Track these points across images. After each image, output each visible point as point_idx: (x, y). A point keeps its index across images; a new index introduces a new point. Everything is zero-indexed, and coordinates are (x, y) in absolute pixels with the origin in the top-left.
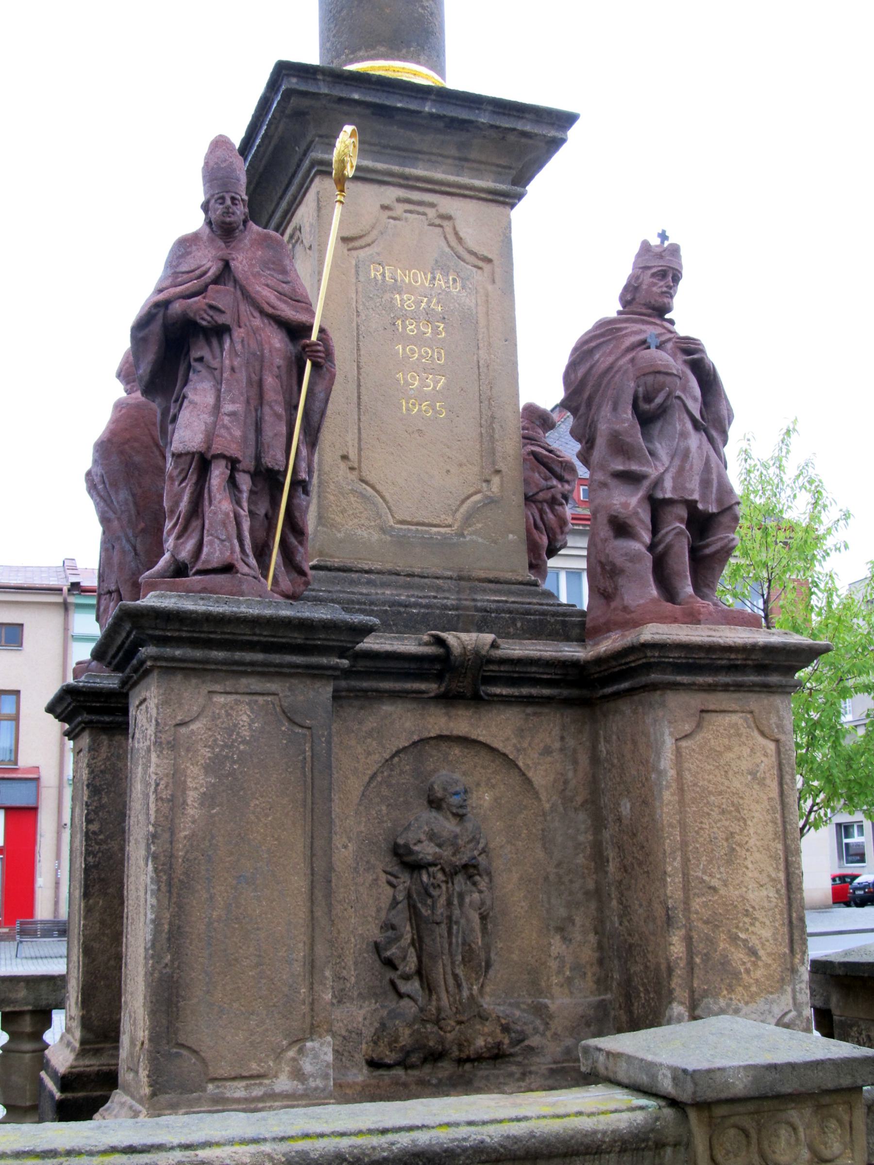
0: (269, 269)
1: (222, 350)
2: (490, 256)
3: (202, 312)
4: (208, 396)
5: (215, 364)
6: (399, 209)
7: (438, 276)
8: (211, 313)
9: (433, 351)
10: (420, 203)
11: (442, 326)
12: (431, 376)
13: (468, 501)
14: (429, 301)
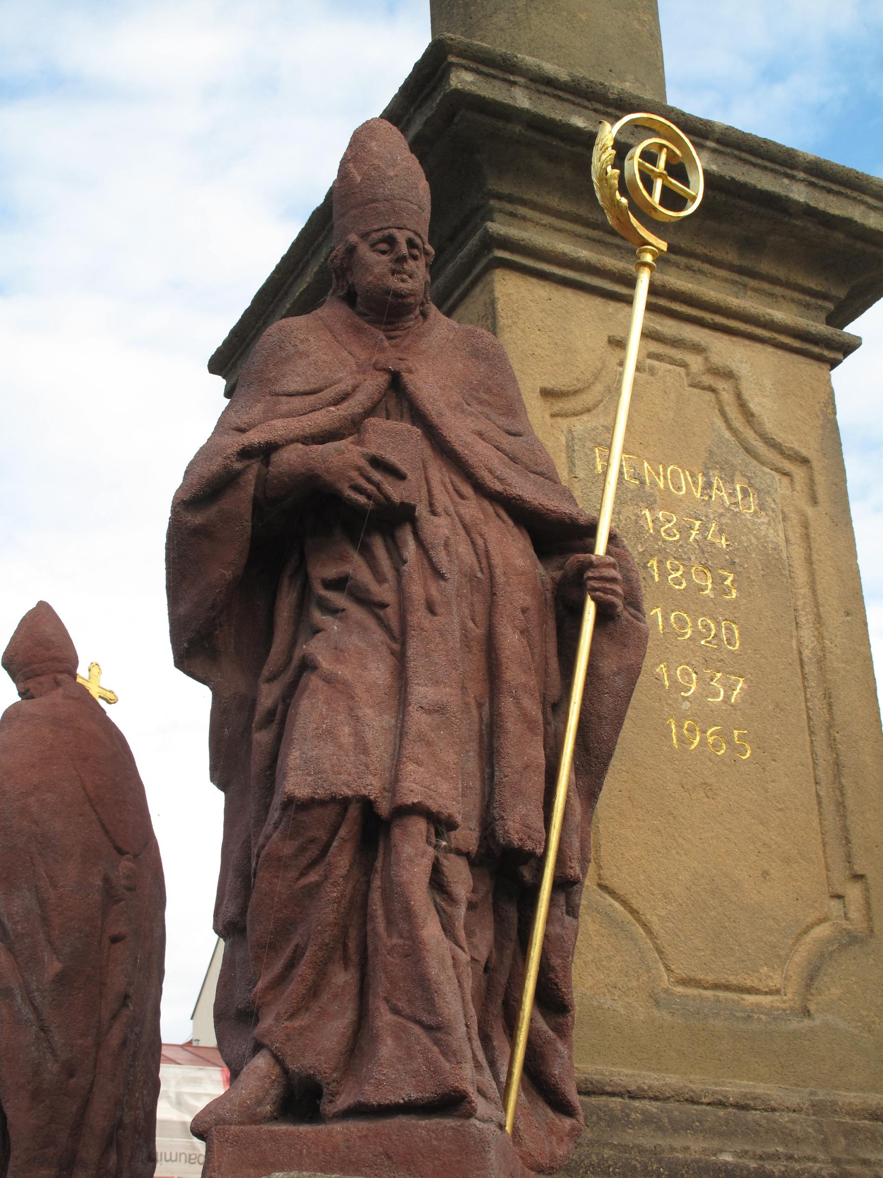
0: (481, 402)
1: (398, 561)
2: (804, 452)
3: (354, 474)
4: (372, 665)
5: (385, 593)
7: (716, 481)
8: (377, 476)
9: (718, 625)
10: (676, 343)
12: (719, 675)
14: (704, 529)
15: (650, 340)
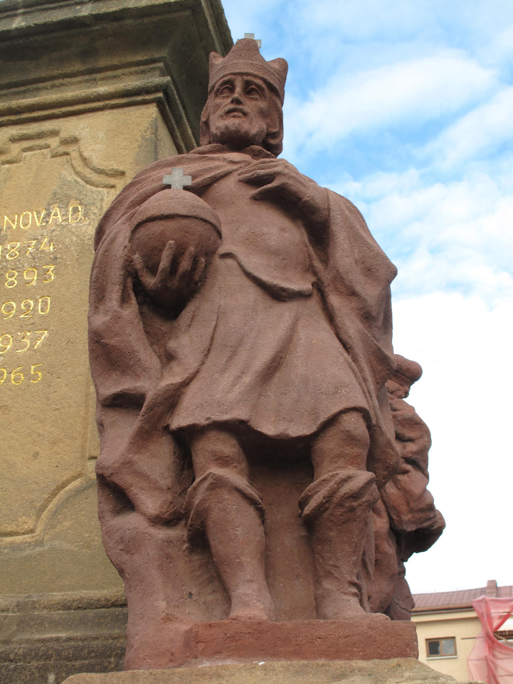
2: (121, 168)
6: (16, 149)
9: (36, 302)
10: (40, 136)
11: (52, 267)
12: (28, 334)
13: (62, 492)
15: (23, 142)
